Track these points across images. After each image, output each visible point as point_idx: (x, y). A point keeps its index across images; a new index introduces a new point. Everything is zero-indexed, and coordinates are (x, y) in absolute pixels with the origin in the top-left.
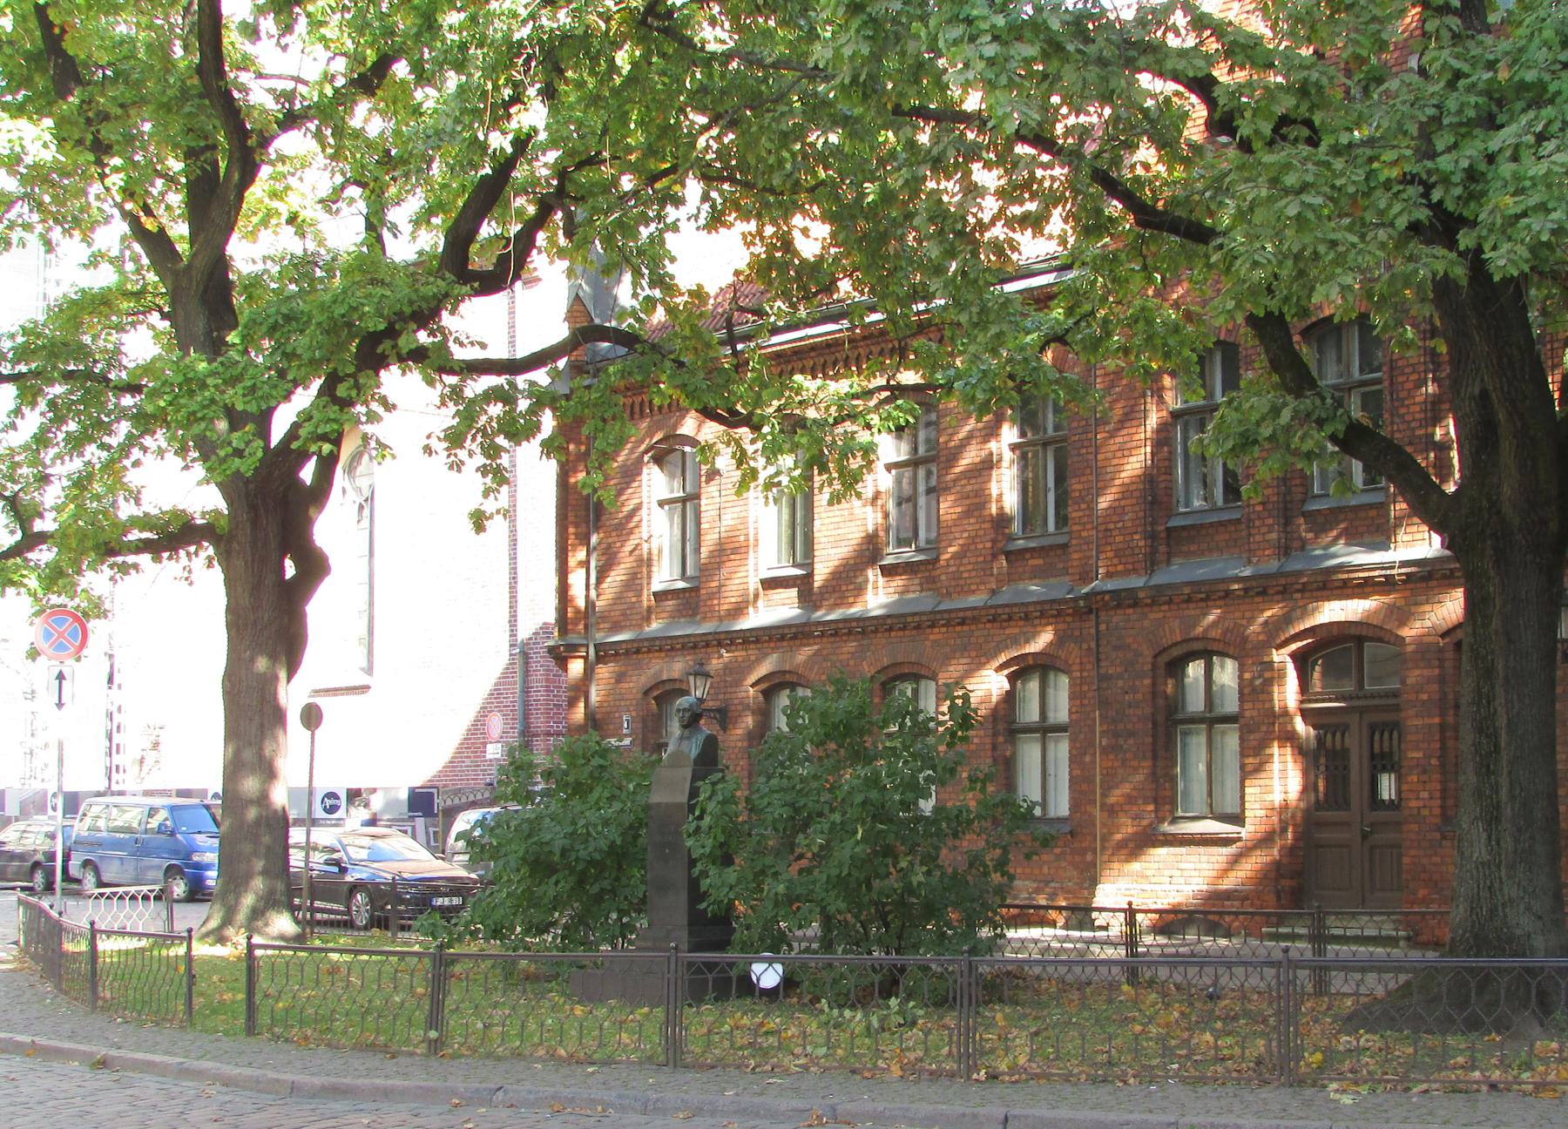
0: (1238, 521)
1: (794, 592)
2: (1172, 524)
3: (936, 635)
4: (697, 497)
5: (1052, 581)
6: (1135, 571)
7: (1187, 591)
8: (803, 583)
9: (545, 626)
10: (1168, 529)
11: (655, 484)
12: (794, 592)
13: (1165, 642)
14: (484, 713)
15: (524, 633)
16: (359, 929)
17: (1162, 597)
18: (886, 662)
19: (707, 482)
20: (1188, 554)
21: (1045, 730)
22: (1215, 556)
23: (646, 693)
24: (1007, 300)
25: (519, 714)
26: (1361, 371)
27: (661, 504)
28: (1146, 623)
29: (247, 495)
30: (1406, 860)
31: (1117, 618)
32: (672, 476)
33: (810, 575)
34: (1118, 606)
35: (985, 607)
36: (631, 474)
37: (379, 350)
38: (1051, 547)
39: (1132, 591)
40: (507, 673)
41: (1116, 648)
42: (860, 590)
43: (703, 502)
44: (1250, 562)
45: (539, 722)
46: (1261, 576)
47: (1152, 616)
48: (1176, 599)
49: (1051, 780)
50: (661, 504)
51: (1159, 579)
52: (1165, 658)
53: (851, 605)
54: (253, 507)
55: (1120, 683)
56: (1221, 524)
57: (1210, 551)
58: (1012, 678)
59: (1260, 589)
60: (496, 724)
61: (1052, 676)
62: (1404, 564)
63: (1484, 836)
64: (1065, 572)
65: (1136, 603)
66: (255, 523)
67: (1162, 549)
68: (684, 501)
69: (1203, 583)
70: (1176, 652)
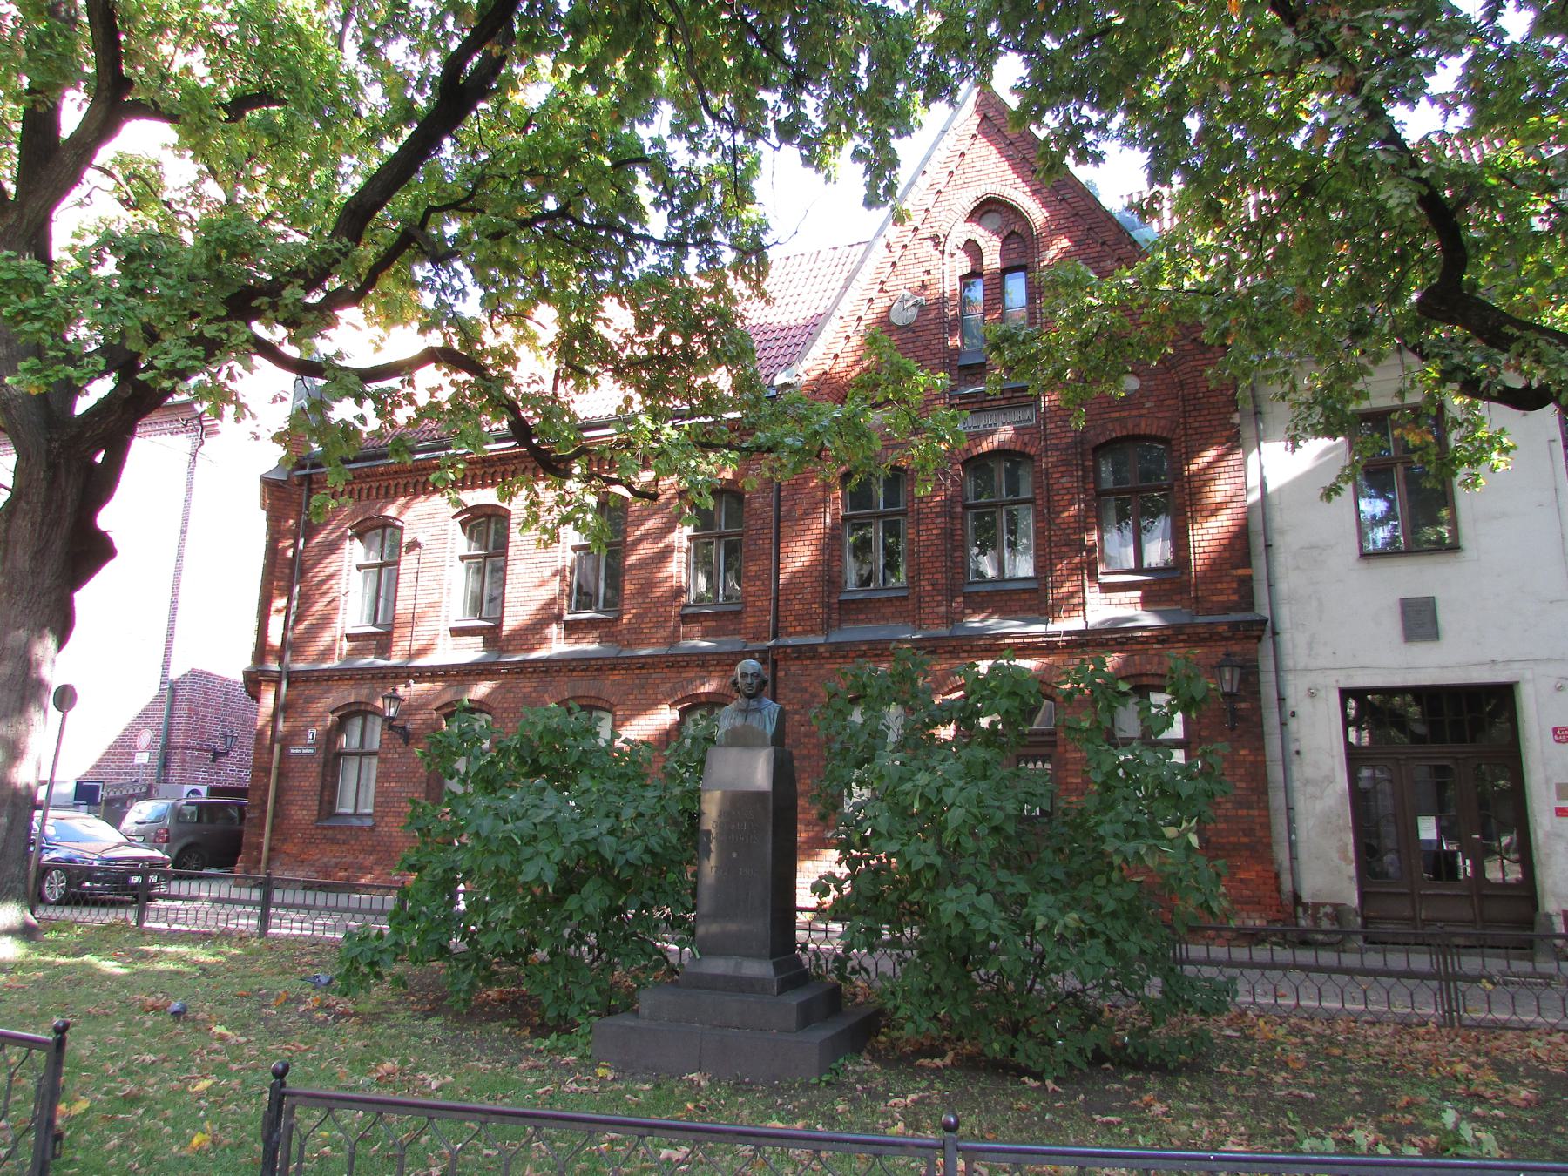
1: (480, 639)
2: (844, 597)
3: (615, 677)
4: (397, 563)
5: (724, 638)
6: (813, 631)
8: (491, 636)
10: (840, 602)
11: (355, 552)
12: (480, 639)
14: (130, 733)
15: (175, 673)
16: (51, 904)
17: (840, 651)
19: (407, 552)
20: (856, 621)
22: (882, 624)
24: (741, 410)
25: (162, 733)
27: (359, 568)
28: (822, 672)
29: (49, 452)
31: (795, 668)
32: (369, 548)
33: (499, 626)
34: (797, 658)
35: (666, 655)
36: (332, 547)
37: (255, 303)
38: (724, 613)
39: (813, 648)
40: (157, 701)
42: (544, 640)
43: (402, 567)
44: (920, 627)
45: (178, 739)
47: (828, 666)
48: (852, 654)
49: (362, 789)
50: (359, 568)
51: (835, 637)
53: (532, 650)
54: (52, 466)
55: (797, 717)
57: (878, 620)
58: (683, 712)
59: (933, 647)
60: (146, 737)
62: (1067, 633)
64: (737, 632)
66: (53, 482)
67: (835, 616)
68: (380, 566)
69: (880, 642)
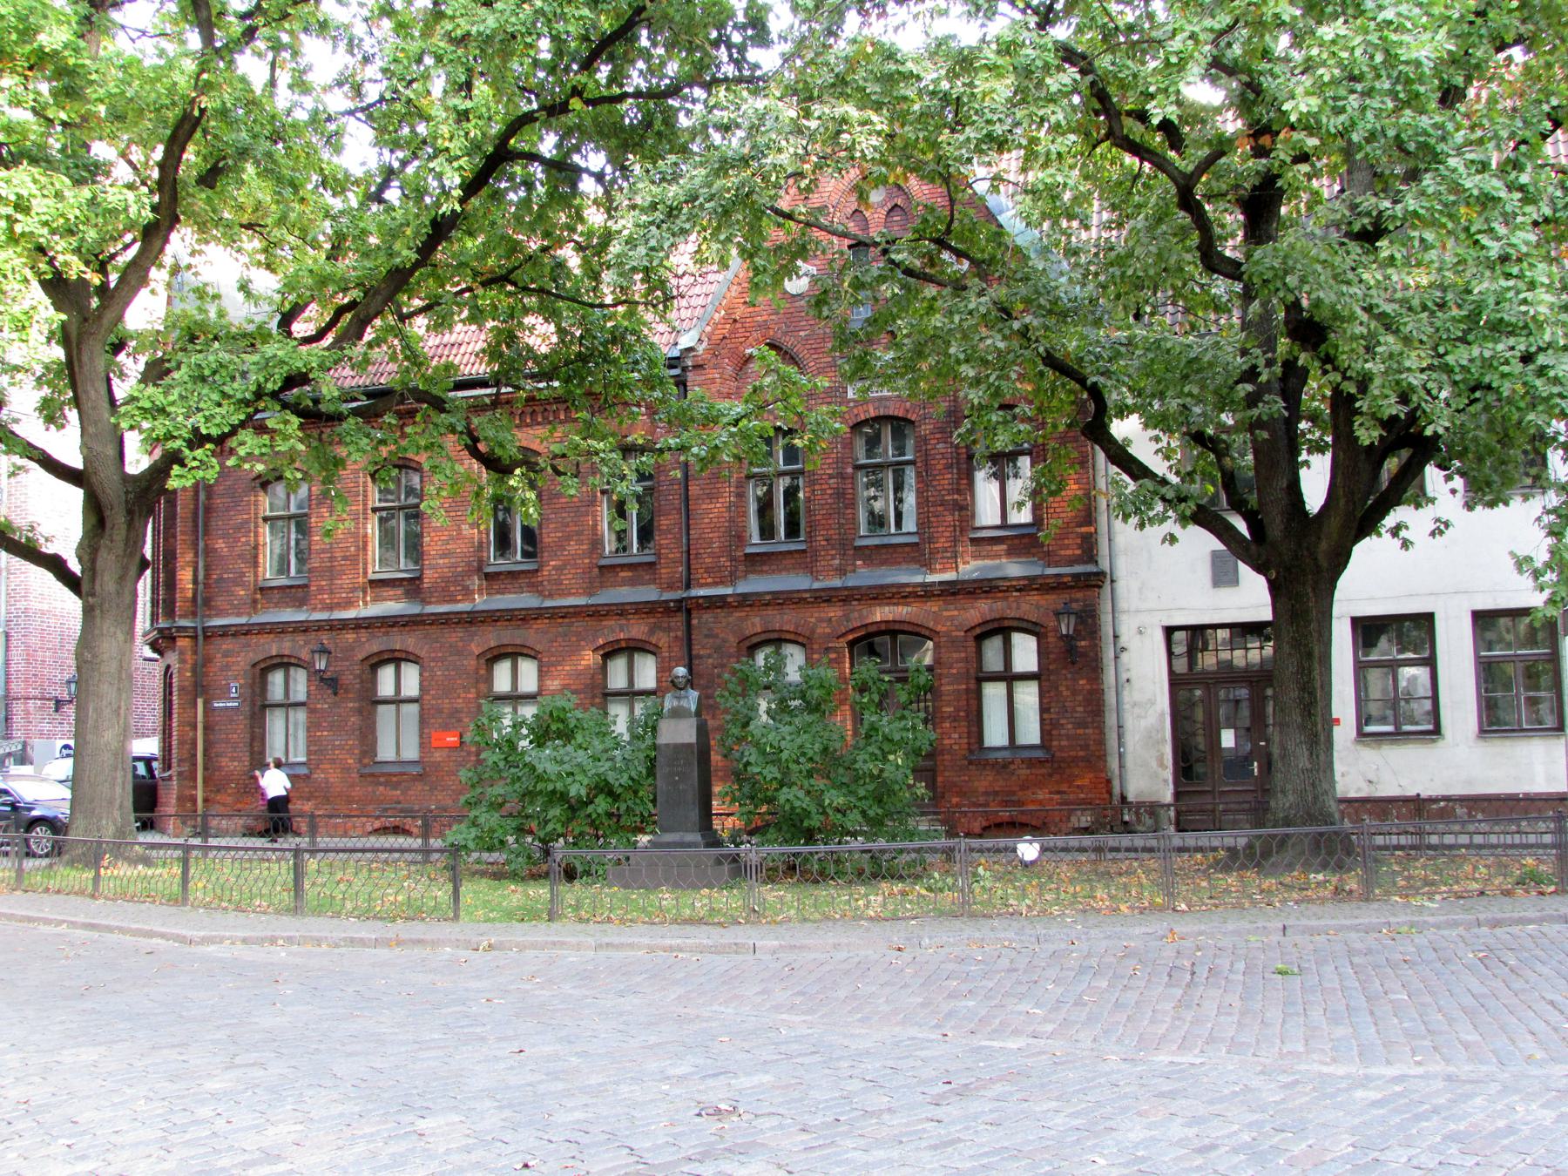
0: (804, 551)
7: (768, 597)
9: (1215, 555)
13: (747, 633)
18: (493, 644)
21: (288, 706)
23: (254, 665)
26: (785, 464)
29: (127, 502)
30: (940, 779)
31: (707, 617)
39: (723, 597)
41: (706, 636)
46: (846, 588)
52: (747, 643)
56: (790, 552)
57: (780, 571)
61: (403, 665)
63: (1306, 753)
65: (729, 605)
70: (755, 640)
